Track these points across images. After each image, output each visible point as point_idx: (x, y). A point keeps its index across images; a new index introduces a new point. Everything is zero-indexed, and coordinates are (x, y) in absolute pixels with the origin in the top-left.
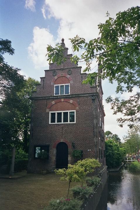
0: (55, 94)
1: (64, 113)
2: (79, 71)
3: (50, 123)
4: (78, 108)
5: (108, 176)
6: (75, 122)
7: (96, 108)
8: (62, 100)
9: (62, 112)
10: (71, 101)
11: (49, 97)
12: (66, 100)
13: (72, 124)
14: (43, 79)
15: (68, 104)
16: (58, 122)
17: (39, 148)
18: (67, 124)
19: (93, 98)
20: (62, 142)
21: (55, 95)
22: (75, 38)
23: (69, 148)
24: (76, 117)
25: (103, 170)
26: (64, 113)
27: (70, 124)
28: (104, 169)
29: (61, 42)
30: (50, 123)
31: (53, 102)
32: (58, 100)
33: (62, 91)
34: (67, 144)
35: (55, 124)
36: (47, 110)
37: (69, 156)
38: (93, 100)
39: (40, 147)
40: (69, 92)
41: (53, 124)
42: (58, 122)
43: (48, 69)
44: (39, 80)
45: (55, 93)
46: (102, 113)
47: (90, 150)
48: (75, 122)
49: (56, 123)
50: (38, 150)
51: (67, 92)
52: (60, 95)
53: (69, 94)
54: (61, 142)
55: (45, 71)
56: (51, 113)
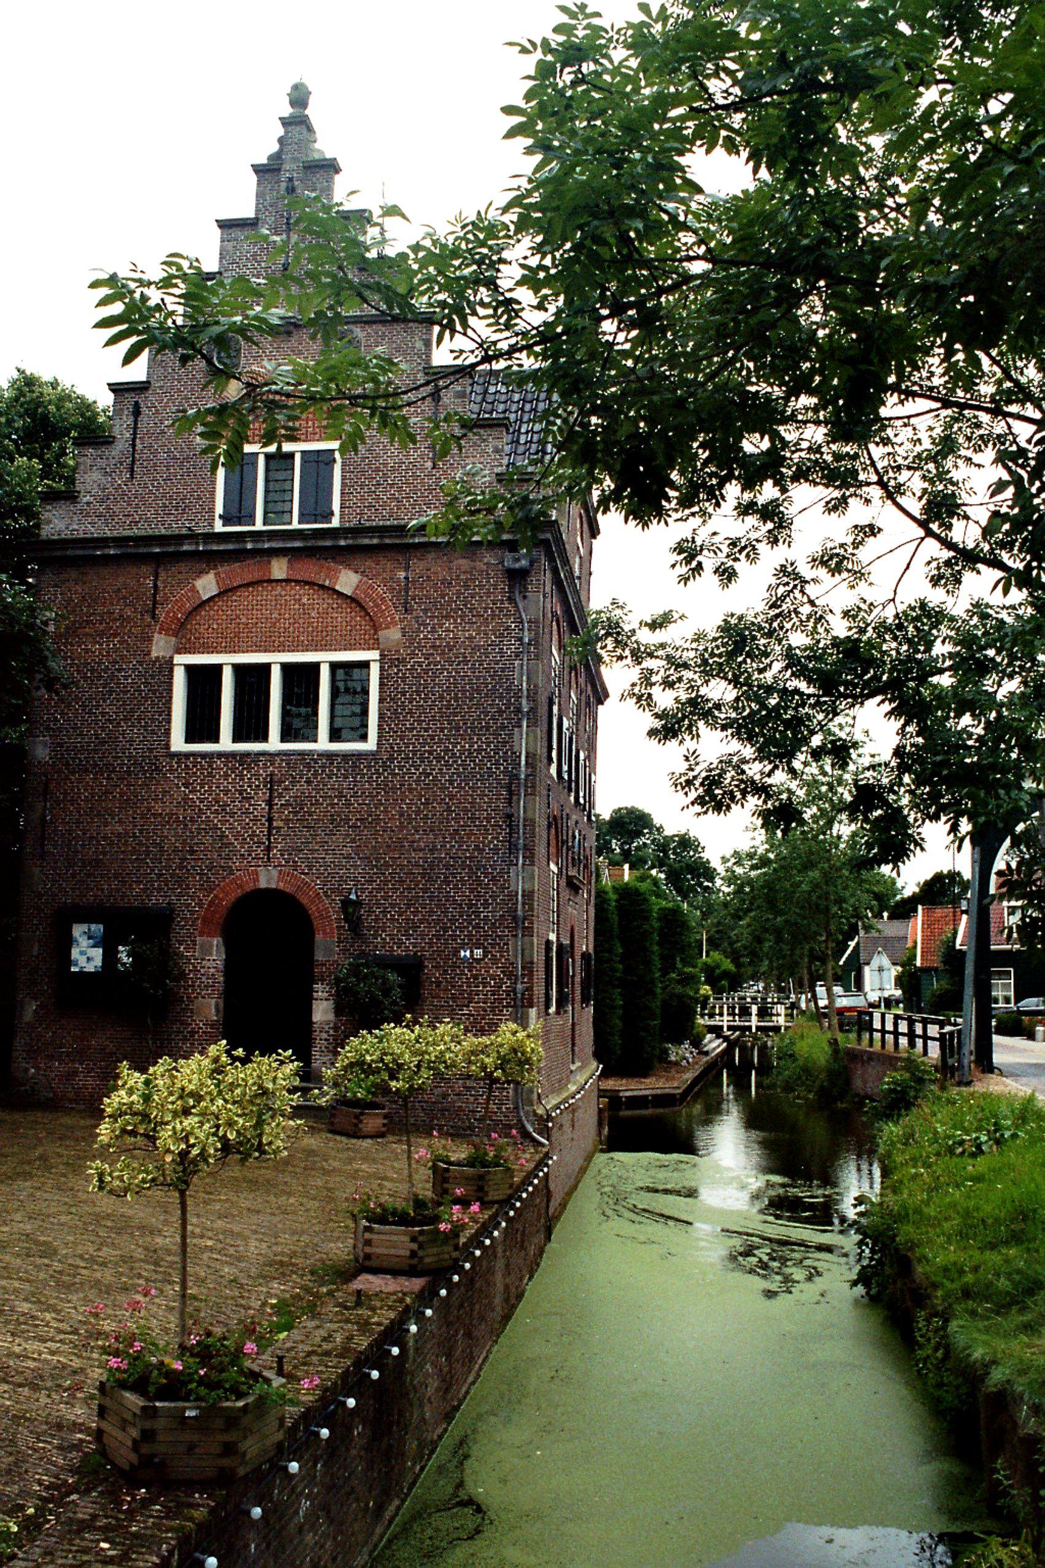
0: (227, 519)
1: (286, 668)
2: (419, 345)
3: (178, 742)
4: (393, 635)
5: (606, 1131)
6: (371, 745)
7: (535, 642)
8: (279, 569)
9: (276, 659)
10: (347, 581)
11: (179, 539)
12: (309, 570)
13: (346, 756)
14: (130, 399)
15: (323, 602)
16: (237, 738)
17: (93, 927)
18: (310, 753)
19: (518, 560)
20: (267, 891)
21: (219, 527)
22: (735, 147)
23: (319, 937)
24: (381, 700)
25: (565, 1095)
26: (288, 669)
27: (330, 756)
28: (573, 1088)
29: (287, 111)
30: (178, 742)
31: (207, 585)
32: (241, 572)
33: (276, 508)
34: (305, 901)
35: (220, 755)
36: (160, 646)
37: (321, 990)
38: (517, 578)
39: (101, 927)
40: (336, 506)
41: (204, 755)
42: (237, 738)
43: (248, 211)
44: (105, 400)
45: (219, 509)
46: (582, 680)
47: (478, 953)
48: (371, 745)
49: (226, 743)
50: (84, 942)
51: (318, 508)
52: (259, 526)
53: (335, 522)
54: (260, 890)
55: (223, 225)
56: (190, 669)
